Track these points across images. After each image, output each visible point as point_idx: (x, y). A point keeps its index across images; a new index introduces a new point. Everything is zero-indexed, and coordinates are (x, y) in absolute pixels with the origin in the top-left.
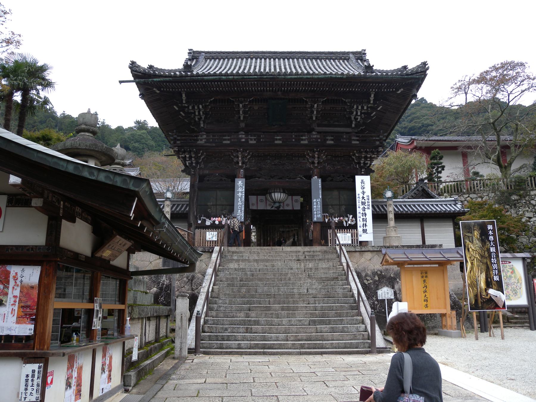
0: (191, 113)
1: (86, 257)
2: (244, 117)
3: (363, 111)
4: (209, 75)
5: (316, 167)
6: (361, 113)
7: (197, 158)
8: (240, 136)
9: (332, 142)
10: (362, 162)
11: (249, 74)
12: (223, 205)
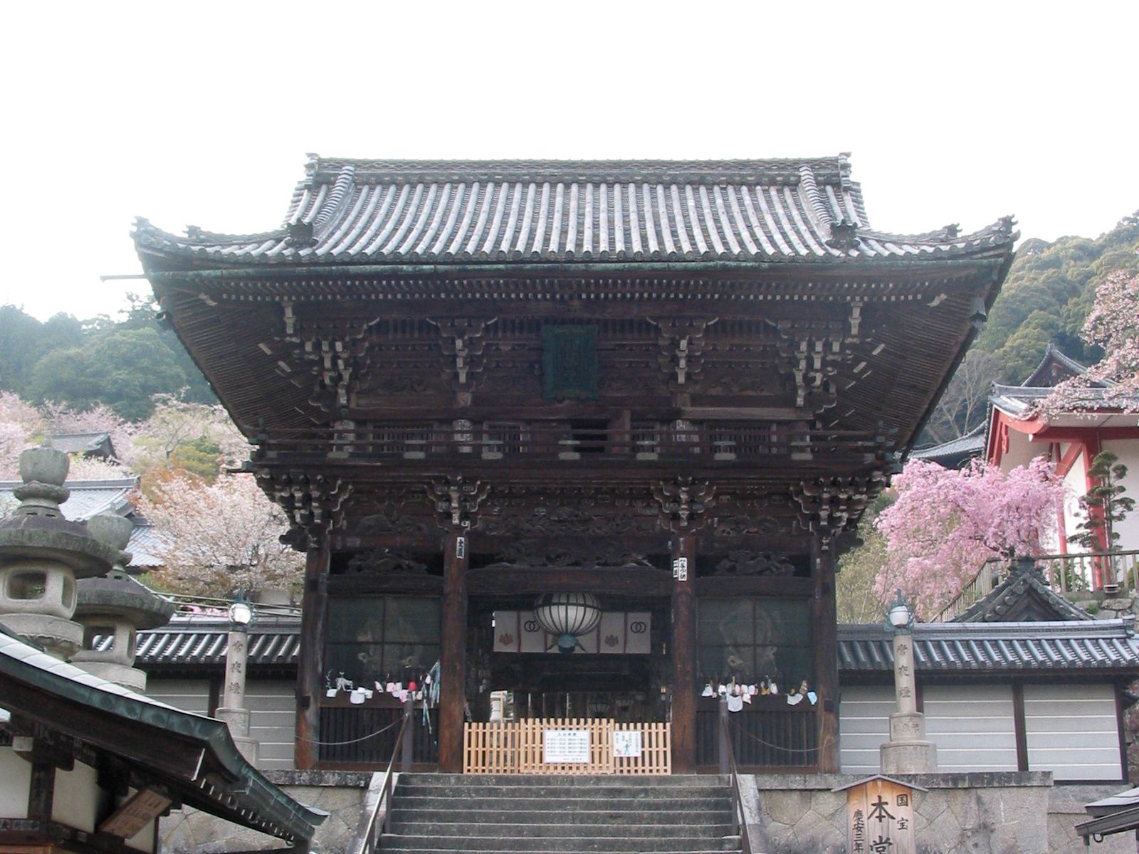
0: (313, 363)
1: (88, 834)
2: (470, 376)
3: (830, 357)
4: (362, 259)
5: (684, 531)
6: (825, 363)
7: (327, 502)
8: (458, 437)
9: (730, 456)
10: (823, 514)
11: (479, 259)
12: (404, 644)
